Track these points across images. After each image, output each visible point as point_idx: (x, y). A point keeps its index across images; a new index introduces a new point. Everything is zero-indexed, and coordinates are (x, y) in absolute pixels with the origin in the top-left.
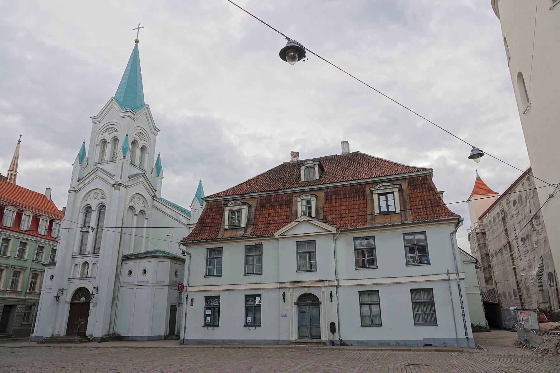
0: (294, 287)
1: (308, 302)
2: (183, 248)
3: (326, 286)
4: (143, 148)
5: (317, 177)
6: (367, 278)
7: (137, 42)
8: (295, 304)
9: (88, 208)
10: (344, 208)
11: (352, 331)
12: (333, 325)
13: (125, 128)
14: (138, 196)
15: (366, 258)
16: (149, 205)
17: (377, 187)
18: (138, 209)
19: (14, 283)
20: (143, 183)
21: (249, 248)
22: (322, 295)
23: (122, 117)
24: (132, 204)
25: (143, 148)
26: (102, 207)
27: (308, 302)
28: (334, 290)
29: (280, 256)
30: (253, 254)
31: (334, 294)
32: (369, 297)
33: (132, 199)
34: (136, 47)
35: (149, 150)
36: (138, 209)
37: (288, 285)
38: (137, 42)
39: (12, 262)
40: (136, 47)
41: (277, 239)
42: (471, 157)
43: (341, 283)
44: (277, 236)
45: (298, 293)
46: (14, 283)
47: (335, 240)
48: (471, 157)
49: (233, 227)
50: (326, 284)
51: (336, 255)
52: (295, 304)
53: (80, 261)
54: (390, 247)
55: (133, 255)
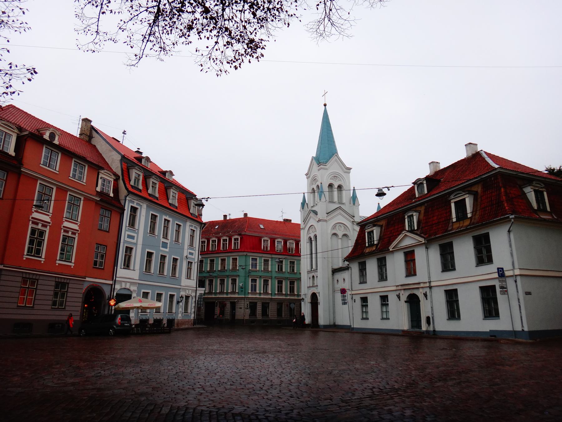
0: (404, 289)
1: (413, 302)
2: (347, 263)
3: (423, 287)
4: (340, 187)
5: (426, 192)
6: (450, 279)
7: (325, 105)
8: (405, 302)
9: (310, 239)
10: (436, 218)
11: (443, 324)
12: (428, 319)
13: (324, 177)
14: (338, 225)
15: (448, 264)
16: (350, 229)
17: (452, 197)
18: (340, 234)
19: (280, 289)
20: (340, 214)
21: (379, 260)
22: (420, 294)
23: (319, 170)
24: (334, 231)
25: (340, 187)
26: (316, 236)
27: (413, 302)
28: (428, 290)
29: (396, 263)
30: (382, 265)
31: (428, 294)
32: (452, 296)
33: (334, 227)
34: (325, 109)
35: (345, 187)
36: (340, 234)
37: (400, 288)
38: (325, 105)
39: (287, 275)
40: (325, 109)
41: (392, 251)
42: (377, 195)
43: (433, 284)
44: (391, 250)
45: (407, 293)
46: (280, 289)
47: (427, 248)
48: (377, 195)
49: (371, 245)
50: (422, 285)
51: (428, 260)
52: (405, 302)
53: (311, 275)
54: (464, 250)
55: (341, 268)
